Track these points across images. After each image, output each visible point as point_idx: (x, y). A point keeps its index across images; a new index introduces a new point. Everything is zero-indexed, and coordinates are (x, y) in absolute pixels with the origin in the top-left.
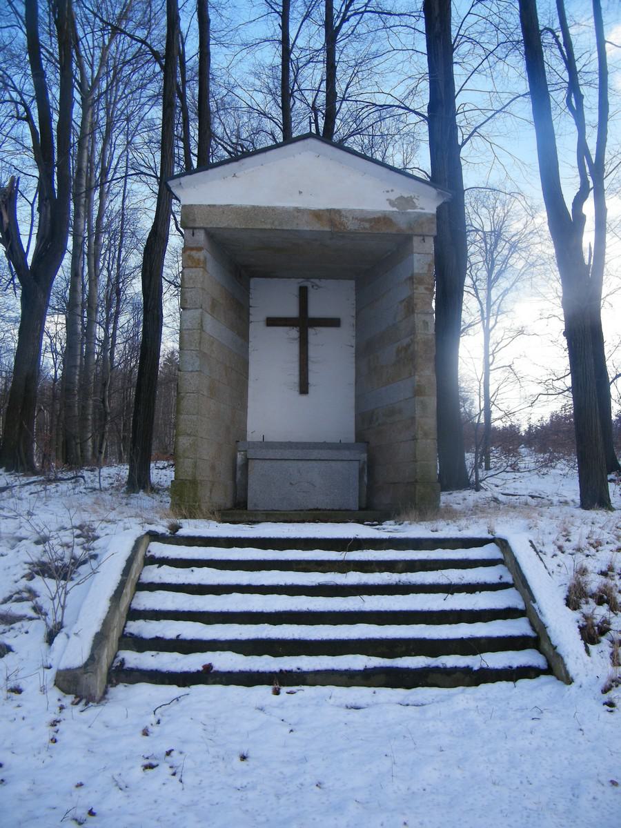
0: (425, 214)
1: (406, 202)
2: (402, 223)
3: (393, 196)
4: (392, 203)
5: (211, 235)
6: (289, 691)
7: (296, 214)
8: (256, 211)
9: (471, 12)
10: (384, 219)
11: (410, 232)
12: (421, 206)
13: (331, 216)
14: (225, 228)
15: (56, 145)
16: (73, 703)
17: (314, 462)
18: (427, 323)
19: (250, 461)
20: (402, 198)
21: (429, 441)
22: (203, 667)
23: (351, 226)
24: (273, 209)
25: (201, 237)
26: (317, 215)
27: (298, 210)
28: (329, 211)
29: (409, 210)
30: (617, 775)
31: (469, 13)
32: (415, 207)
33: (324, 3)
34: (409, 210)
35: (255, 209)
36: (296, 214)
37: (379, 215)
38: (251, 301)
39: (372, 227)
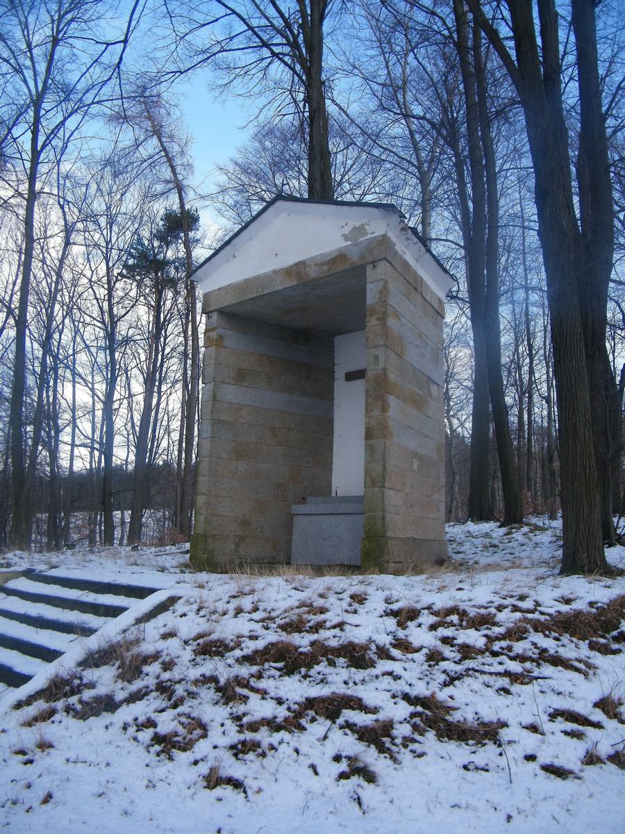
0: (376, 237)
1: (359, 230)
2: (354, 256)
3: (347, 230)
4: (346, 238)
5: (222, 312)
6: (569, 730)
7: (273, 276)
8: (248, 283)
9: (122, 44)
10: (341, 257)
11: (362, 262)
12: (372, 231)
13: (297, 270)
14: (227, 307)
15: (576, 199)
16: (504, 725)
17: (342, 516)
18: (378, 357)
19: (295, 517)
20: (355, 228)
21: (376, 489)
22: (306, 699)
23: (313, 273)
24: (258, 277)
25: (215, 316)
26: (288, 272)
27: (275, 272)
28: (297, 264)
29: (361, 239)
30: (222, 832)
31: (125, 41)
32: (366, 234)
33: (465, 3)
34: (361, 239)
35: (246, 281)
36: (273, 276)
37: (336, 254)
38: (335, 359)
39: (329, 268)
